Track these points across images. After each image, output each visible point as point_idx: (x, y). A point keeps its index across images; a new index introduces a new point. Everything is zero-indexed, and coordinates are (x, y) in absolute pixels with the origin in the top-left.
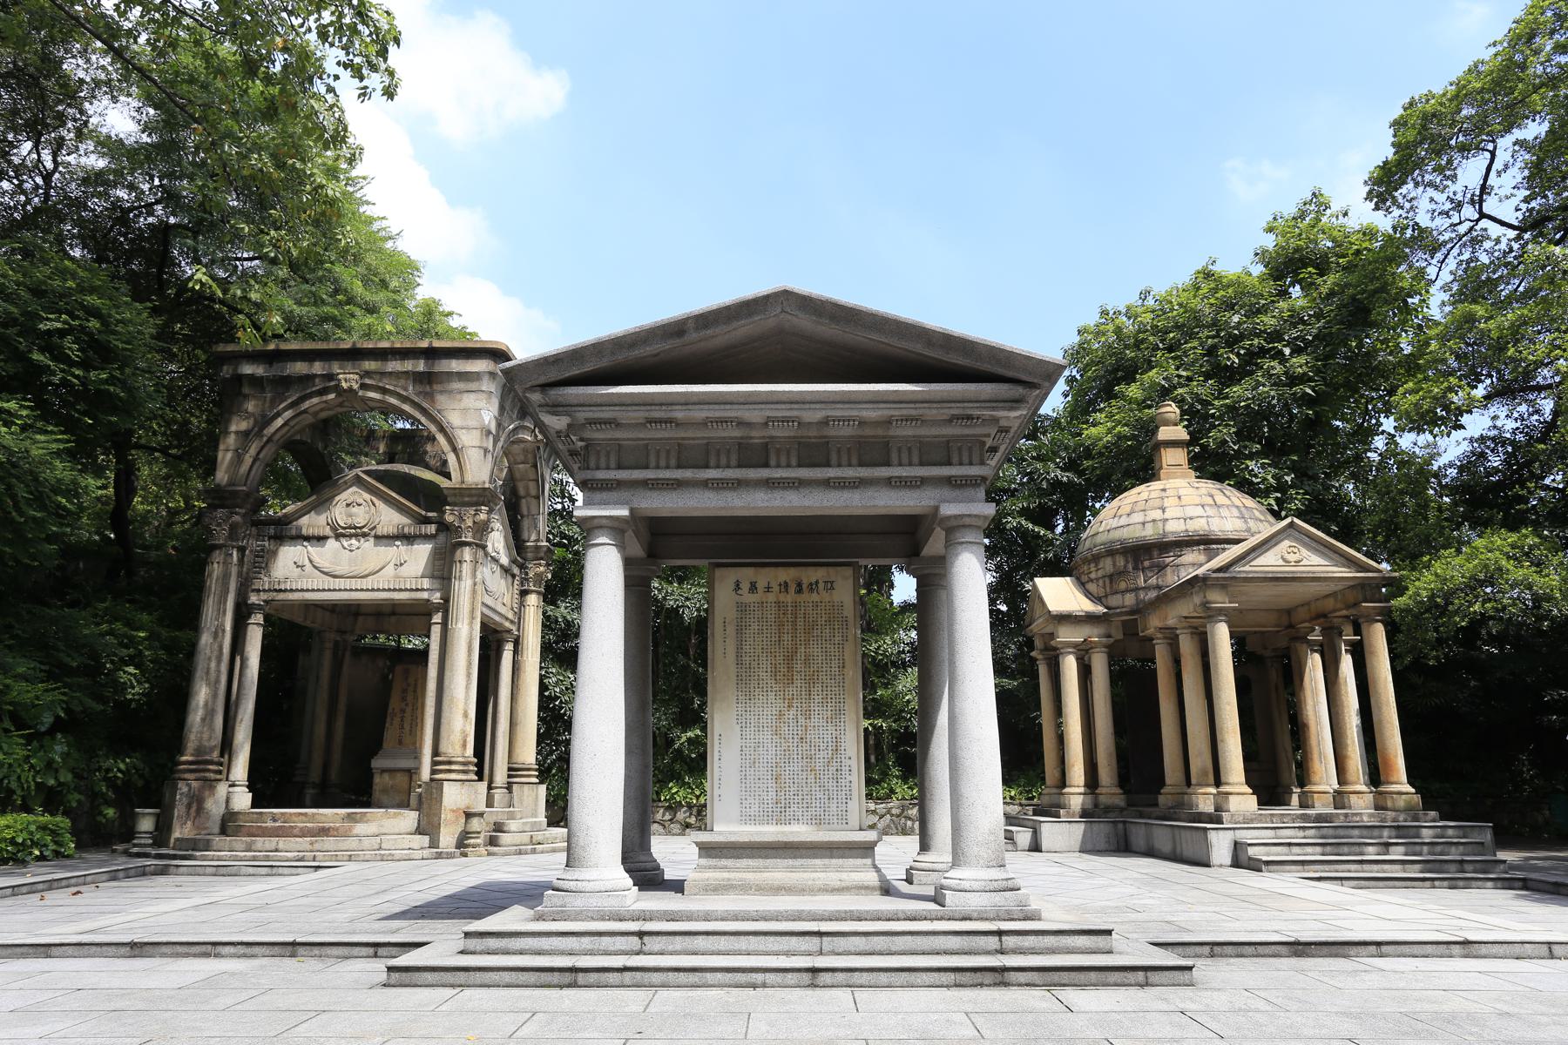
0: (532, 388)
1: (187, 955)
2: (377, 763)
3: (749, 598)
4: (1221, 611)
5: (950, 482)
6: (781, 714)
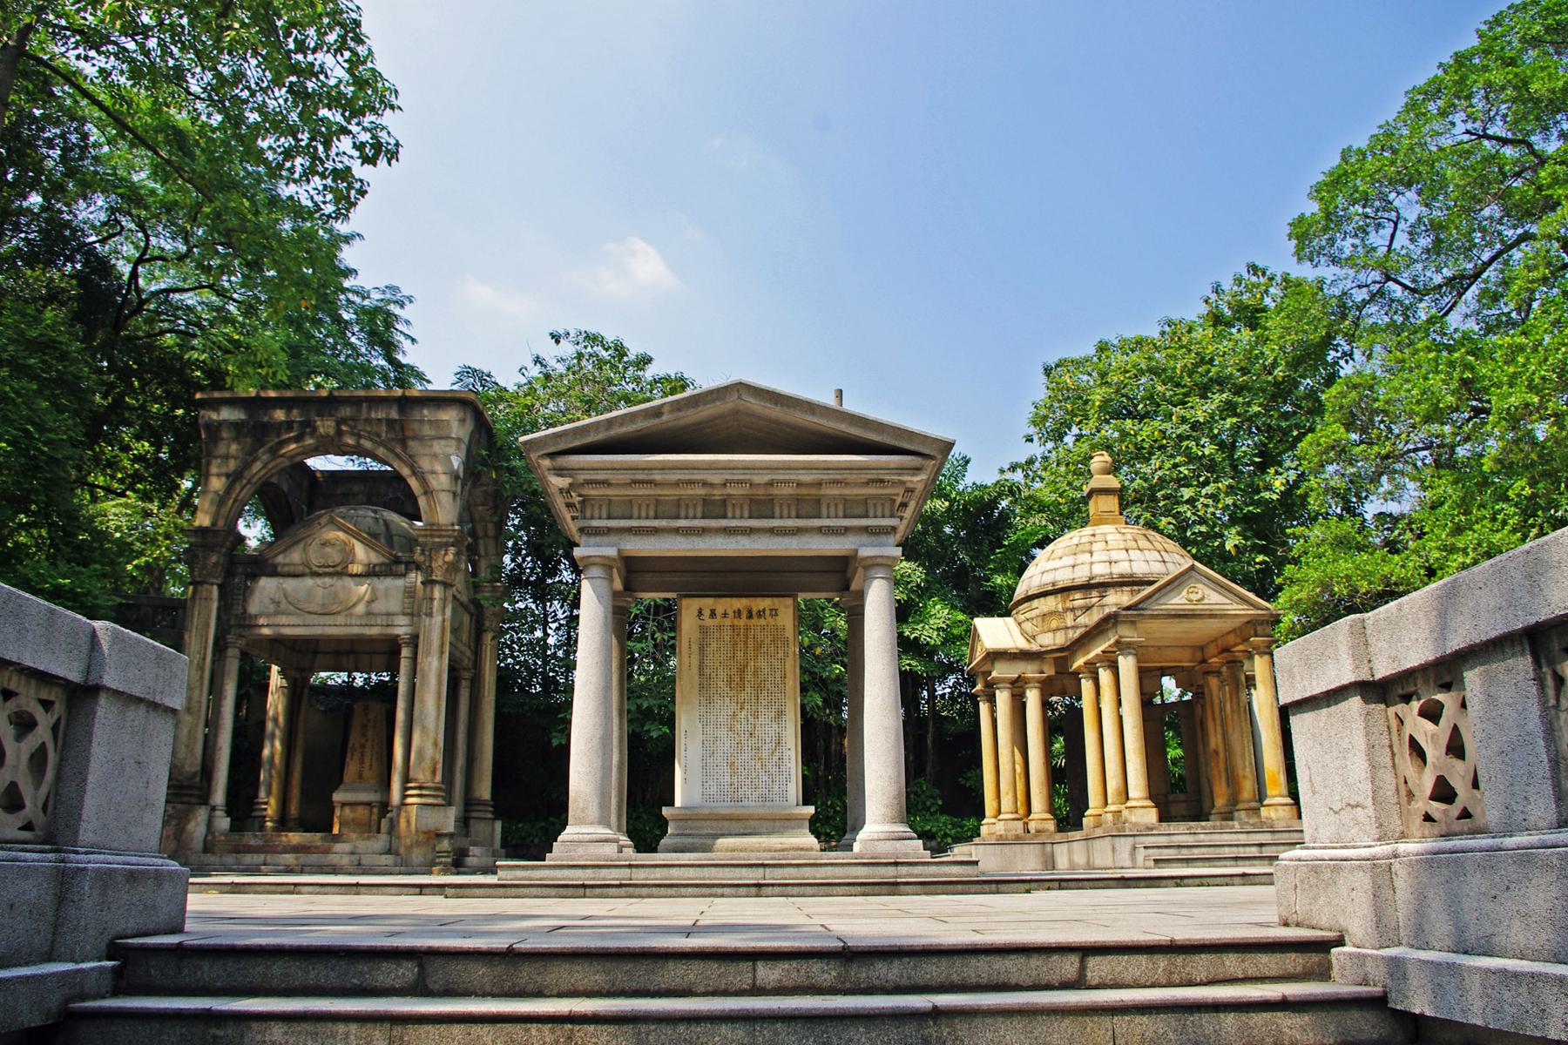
0: (542, 457)
1: (275, 893)
2: (337, 797)
3: (709, 622)
4: (1129, 645)
5: (866, 530)
6: (734, 715)
